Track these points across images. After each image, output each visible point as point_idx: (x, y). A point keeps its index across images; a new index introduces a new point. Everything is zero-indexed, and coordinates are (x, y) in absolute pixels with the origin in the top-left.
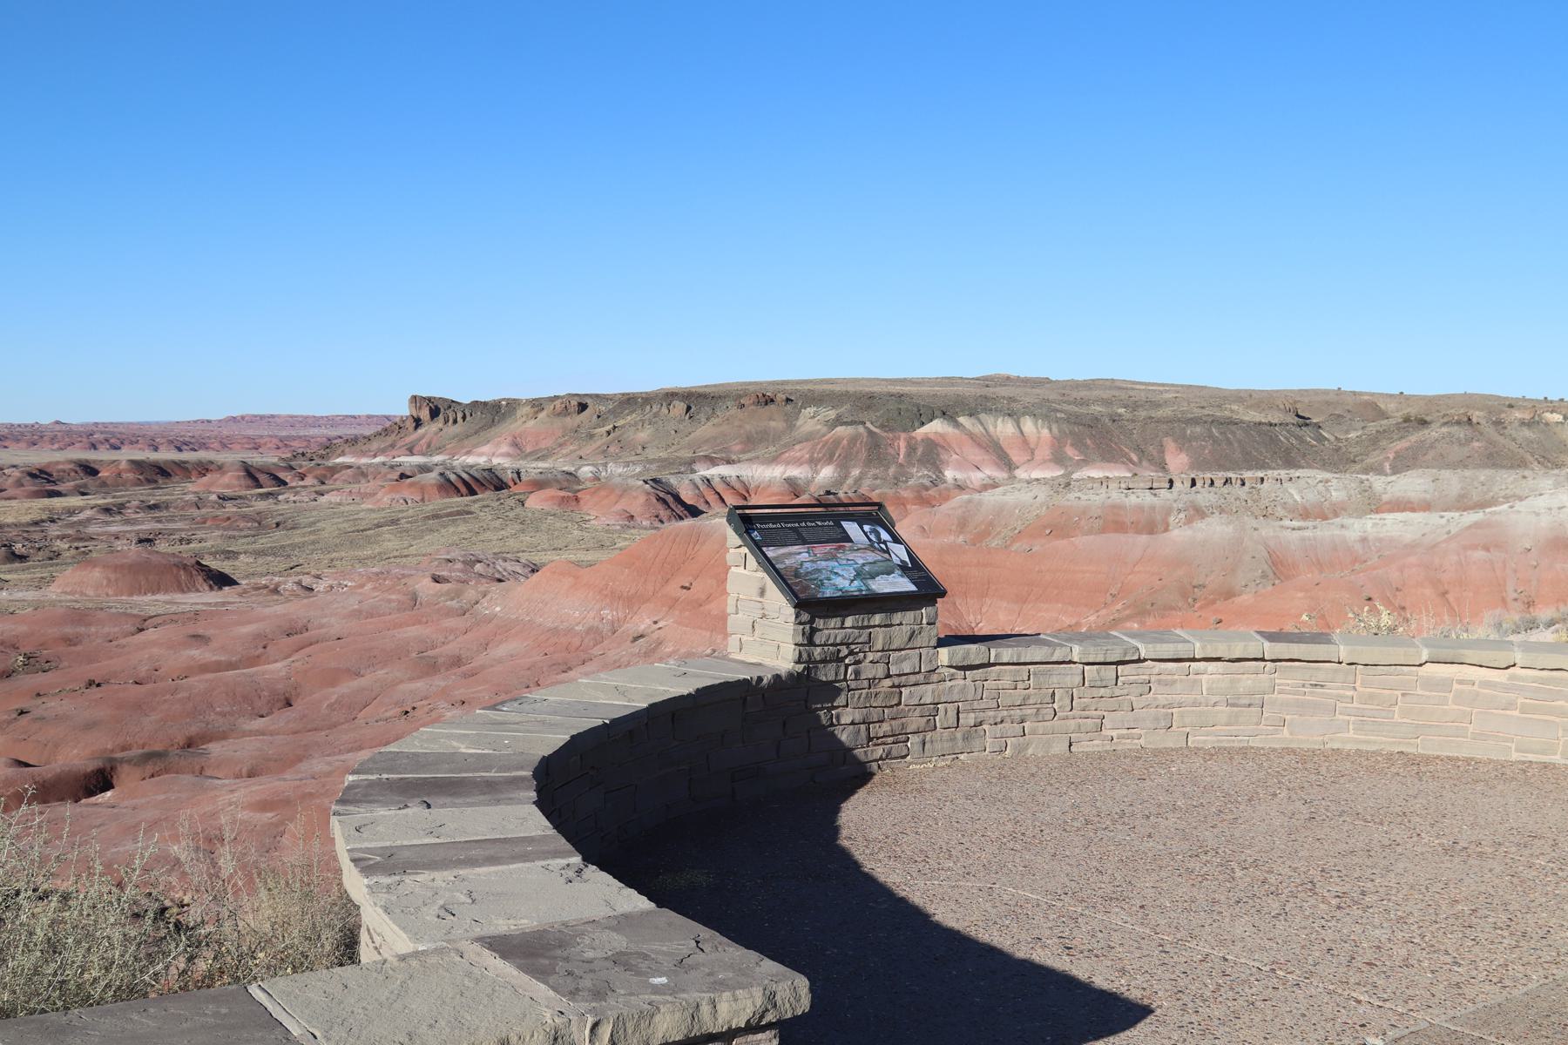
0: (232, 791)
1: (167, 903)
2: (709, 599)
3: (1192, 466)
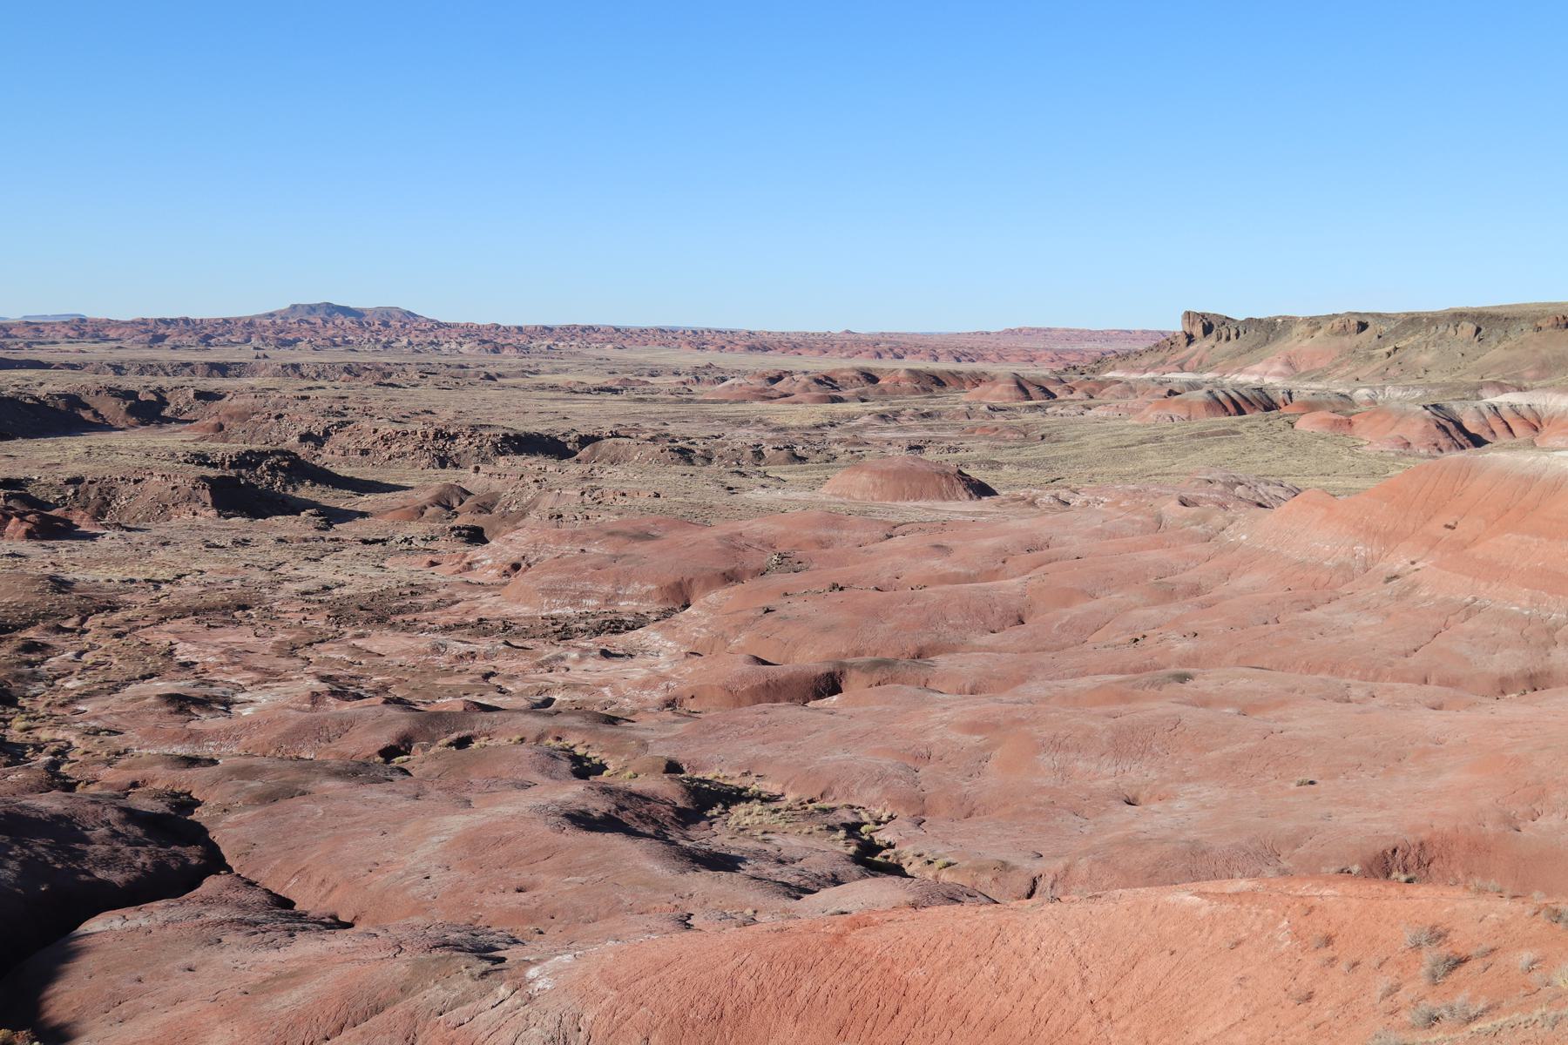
0: (945, 709)
1: (865, 817)
2: (1474, 541)
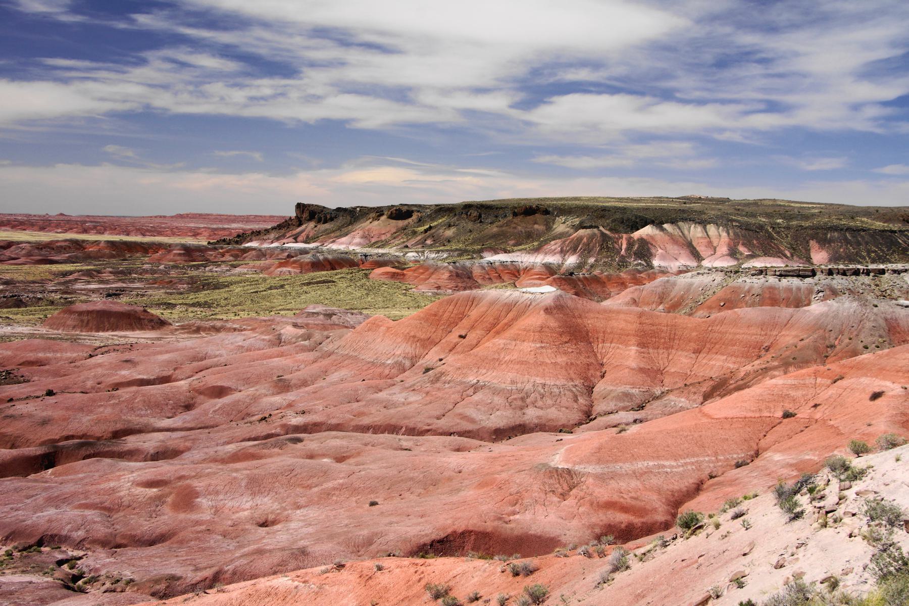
3: (830, 261)
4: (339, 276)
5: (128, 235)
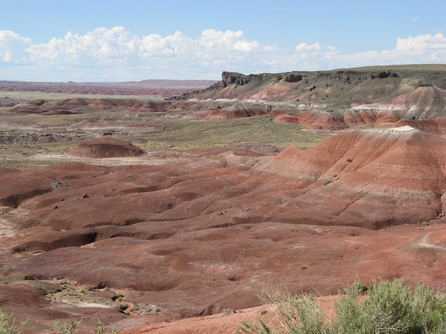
4: (253, 121)
5: (112, 94)
